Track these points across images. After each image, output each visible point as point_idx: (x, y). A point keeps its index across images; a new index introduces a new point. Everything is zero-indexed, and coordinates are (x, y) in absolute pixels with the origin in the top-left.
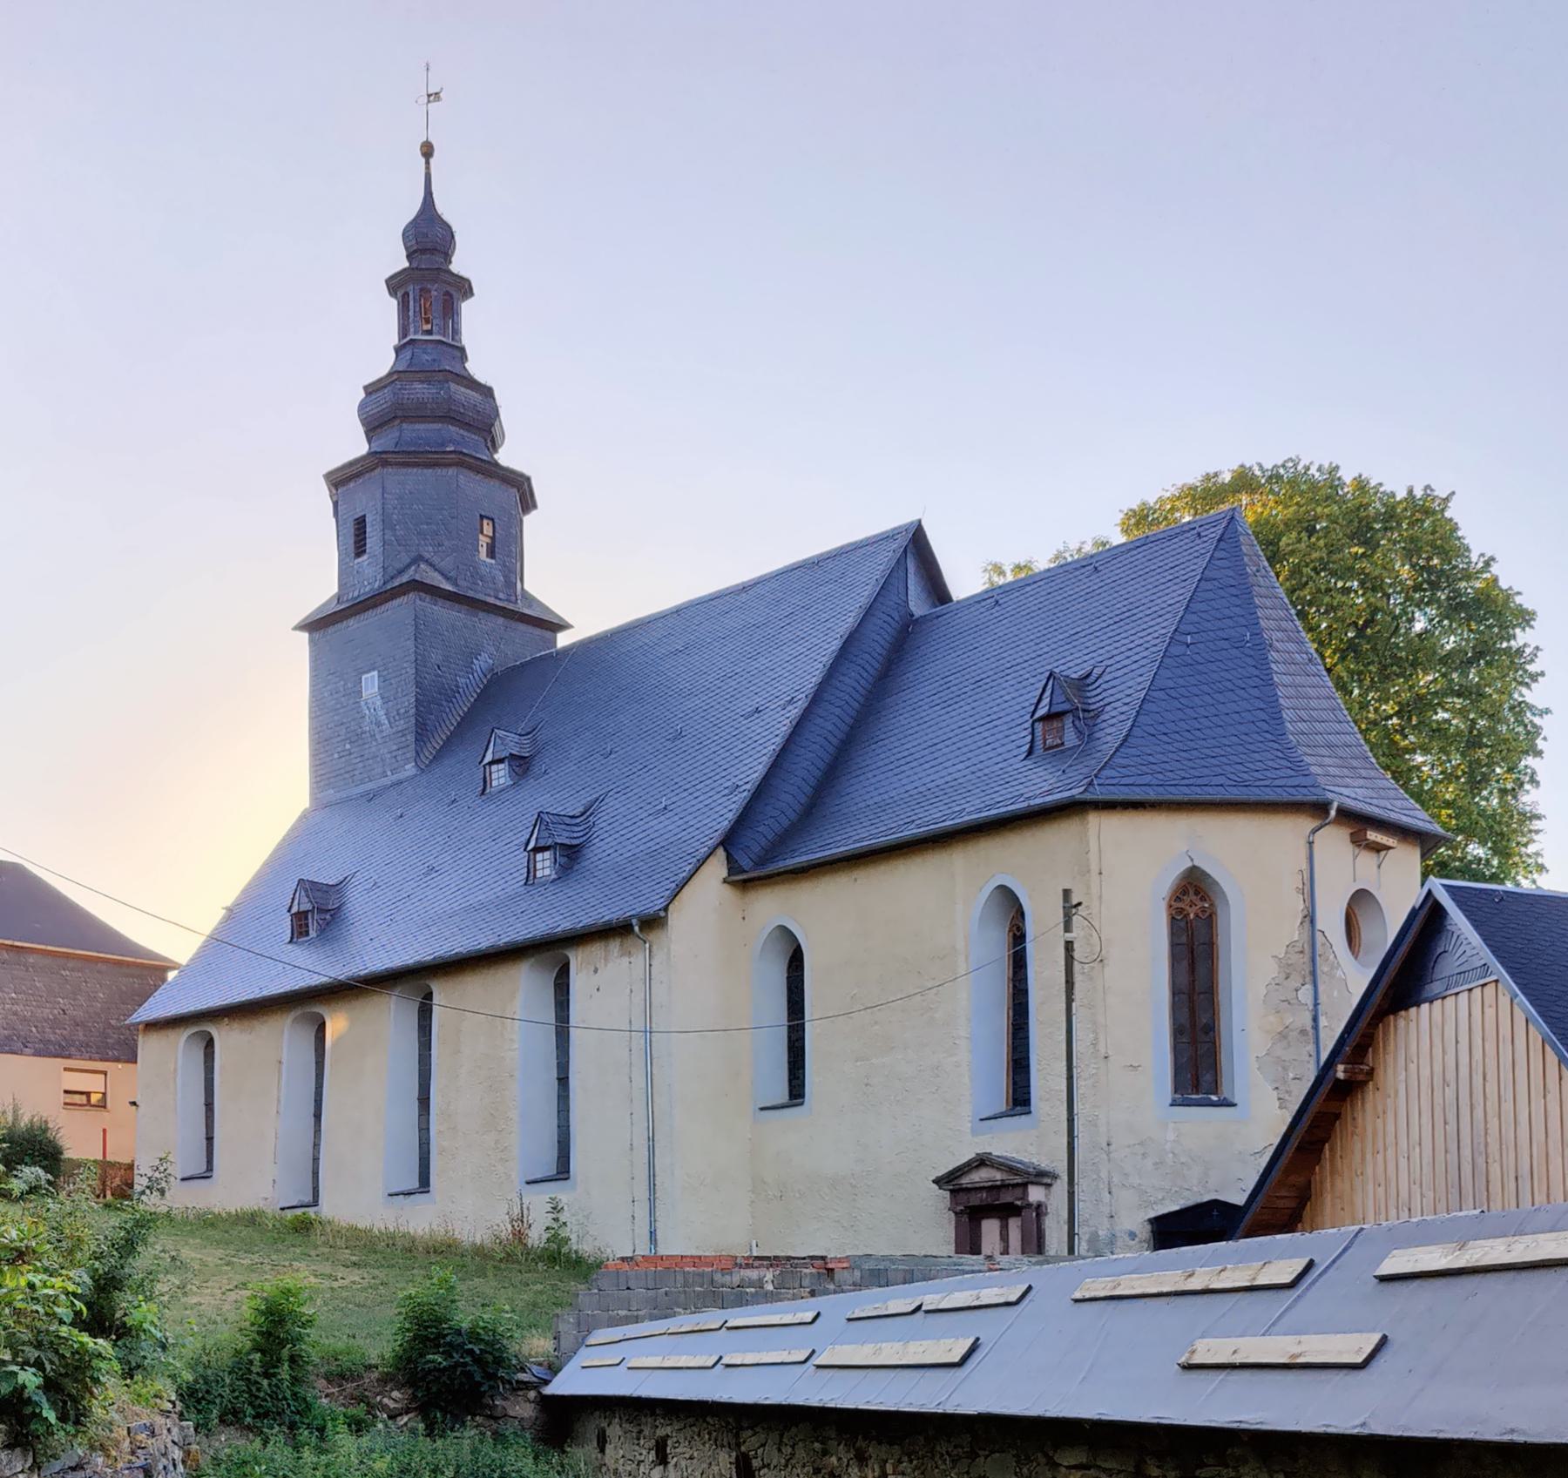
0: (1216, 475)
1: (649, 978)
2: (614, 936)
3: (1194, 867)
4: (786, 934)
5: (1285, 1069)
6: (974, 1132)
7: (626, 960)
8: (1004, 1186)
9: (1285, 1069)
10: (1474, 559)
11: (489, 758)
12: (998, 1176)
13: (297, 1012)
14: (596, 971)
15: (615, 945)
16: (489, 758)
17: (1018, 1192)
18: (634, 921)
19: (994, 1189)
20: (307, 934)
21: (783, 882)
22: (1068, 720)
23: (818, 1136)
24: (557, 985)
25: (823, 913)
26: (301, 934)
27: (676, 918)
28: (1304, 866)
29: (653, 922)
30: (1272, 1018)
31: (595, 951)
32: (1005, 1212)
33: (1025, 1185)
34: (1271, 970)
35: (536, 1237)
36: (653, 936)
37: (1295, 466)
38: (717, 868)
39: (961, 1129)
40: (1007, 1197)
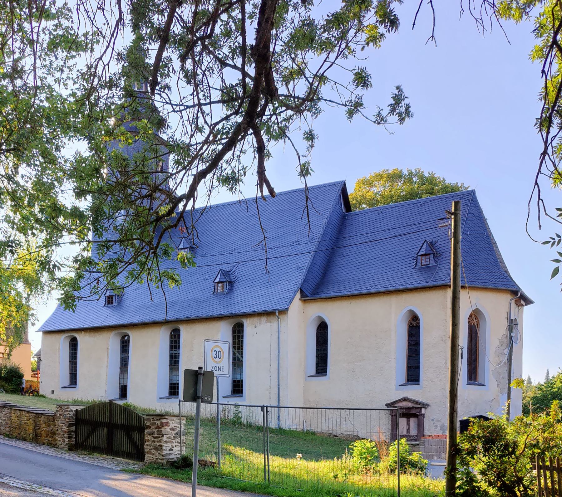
0: (387, 171)
1: (279, 331)
2: (264, 315)
3: (477, 309)
4: (320, 317)
5: (499, 375)
6: (397, 389)
7: (269, 324)
8: (413, 408)
9: (499, 375)
10: (171, 187)
11: (181, 247)
12: (410, 405)
13: (117, 331)
14: (255, 327)
15: (264, 319)
16: (181, 247)
17: (418, 410)
18: (277, 312)
19: (409, 409)
20: (112, 303)
21: (321, 301)
22: (432, 256)
23: (327, 389)
24: (234, 332)
25: (337, 314)
26: (109, 303)
27: (289, 312)
28: (508, 311)
29: (283, 312)
30: (497, 359)
31: (256, 320)
32: (415, 416)
33: (421, 408)
34: (497, 343)
35: (231, 415)
36: (282, 317)
37: (419, 171)
38: (298, 295)
39: (393, 388)
40: (413, 412)
